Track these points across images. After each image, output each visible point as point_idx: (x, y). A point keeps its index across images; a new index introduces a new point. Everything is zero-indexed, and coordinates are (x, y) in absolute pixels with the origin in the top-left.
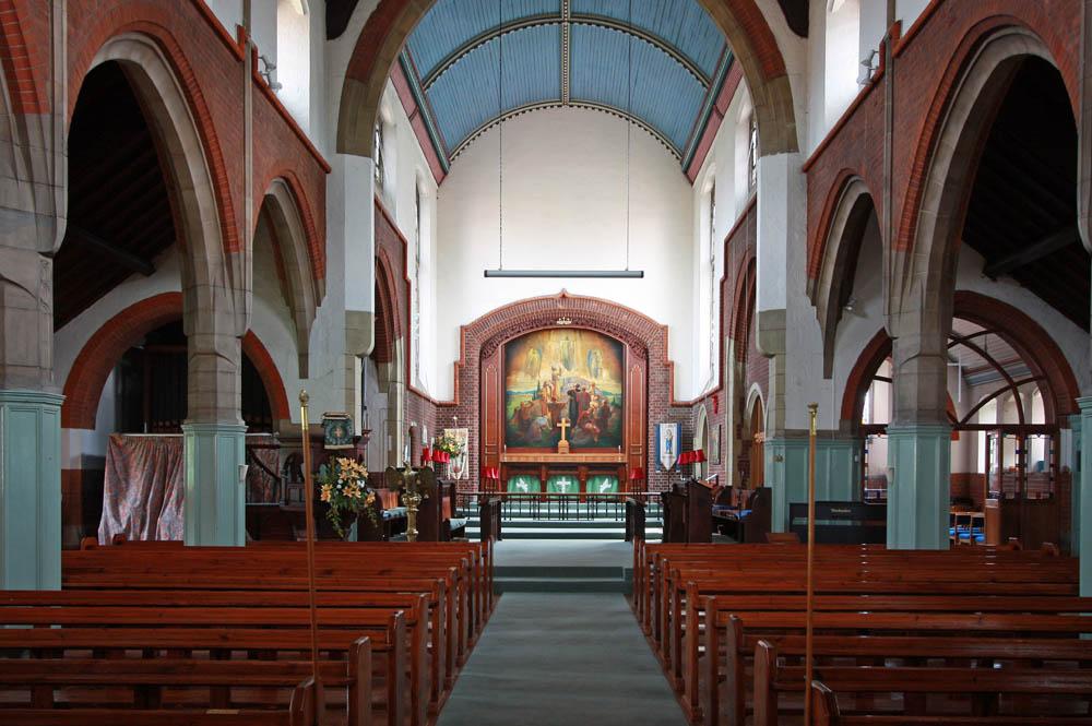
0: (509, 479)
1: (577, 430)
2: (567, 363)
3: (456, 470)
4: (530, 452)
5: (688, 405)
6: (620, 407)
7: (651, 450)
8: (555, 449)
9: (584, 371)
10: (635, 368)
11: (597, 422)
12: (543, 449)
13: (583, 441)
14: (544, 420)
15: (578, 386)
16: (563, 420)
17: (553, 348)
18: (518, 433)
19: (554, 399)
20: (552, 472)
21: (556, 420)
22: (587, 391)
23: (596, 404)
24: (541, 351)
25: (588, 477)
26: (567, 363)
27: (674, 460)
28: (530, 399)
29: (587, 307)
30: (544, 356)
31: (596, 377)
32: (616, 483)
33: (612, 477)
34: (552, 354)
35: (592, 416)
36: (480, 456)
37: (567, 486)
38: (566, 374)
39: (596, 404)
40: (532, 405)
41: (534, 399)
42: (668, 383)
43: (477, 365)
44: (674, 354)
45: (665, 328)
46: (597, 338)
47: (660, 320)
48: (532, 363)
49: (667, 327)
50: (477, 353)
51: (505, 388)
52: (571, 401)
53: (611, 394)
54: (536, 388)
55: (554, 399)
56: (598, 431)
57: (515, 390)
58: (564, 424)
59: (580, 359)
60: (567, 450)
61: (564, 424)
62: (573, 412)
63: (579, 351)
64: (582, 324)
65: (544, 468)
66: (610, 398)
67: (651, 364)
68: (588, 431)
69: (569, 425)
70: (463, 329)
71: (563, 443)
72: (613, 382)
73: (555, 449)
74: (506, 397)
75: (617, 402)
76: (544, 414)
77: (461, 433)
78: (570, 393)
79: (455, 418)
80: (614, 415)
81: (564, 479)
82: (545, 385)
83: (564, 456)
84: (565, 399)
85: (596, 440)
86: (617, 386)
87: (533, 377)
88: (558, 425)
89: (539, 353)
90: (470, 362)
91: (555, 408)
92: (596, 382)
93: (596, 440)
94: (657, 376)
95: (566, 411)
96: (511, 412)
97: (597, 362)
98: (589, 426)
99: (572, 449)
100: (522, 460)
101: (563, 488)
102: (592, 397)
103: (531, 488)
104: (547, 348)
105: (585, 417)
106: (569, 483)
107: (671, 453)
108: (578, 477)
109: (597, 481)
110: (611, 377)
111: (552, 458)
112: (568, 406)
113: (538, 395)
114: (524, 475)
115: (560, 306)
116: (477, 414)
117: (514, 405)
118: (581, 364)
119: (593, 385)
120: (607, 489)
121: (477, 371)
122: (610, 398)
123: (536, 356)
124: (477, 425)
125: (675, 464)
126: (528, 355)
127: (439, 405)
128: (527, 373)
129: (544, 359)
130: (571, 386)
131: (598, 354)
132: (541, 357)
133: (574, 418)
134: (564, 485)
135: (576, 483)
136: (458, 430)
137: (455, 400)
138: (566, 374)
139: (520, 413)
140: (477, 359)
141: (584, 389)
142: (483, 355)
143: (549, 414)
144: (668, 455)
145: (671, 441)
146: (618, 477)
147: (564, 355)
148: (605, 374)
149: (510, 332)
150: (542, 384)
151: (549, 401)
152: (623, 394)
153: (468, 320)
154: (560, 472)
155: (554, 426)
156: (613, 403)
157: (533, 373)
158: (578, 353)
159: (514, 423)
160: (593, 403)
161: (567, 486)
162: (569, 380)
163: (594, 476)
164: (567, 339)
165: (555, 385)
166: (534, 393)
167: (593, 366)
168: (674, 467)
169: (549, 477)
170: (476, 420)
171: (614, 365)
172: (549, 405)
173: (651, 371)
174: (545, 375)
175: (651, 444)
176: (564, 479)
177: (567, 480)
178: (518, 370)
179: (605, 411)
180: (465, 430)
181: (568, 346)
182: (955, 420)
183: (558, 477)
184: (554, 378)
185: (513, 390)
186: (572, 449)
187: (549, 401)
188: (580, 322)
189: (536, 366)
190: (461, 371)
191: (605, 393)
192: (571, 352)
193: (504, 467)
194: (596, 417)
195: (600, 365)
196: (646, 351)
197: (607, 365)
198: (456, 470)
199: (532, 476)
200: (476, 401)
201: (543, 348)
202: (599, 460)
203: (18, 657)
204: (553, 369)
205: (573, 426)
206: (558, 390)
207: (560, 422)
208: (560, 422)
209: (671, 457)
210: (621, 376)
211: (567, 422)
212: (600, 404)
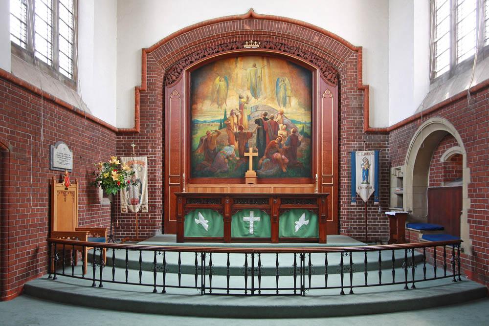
0: (185, 213)
1: (264, 160)
2: (255, 92)
3: (134, 202)
4: (215, 183)
5: (385, 132)
6: (310, 136)
7: (344, 181)
8: (242, 180)
9: (272, 99)
10: (326, 96)
11: (286, 152)
12: (229, 180)
13: (272, 171)
14: (230, 150)
15: (266, 114)
16: (251, 149)
17: (240, 76)
18: (205, 162)
19: (241, 128)
20: (238, 205)
21: (244, 149)
22: (275, 120)
23: (285, 133)
24: (228, 79)
25: (281, 212)
26: (255, 92)
27: (372, 191)
28: (217, 129)
29: (276, 27)
30: (231, 84)
31: (284, 105)
32: (314, 219)
33: (310, 213)
34: (240, 81)
35: (281, 146)
36: (163, 186)
37: (255, 222)
38: (253, 102)
39: (285, 133)
40: (219, 133)
41: (221, 128)
42: (364, 108)
43: (159, 91)
44: (370, 78)
45: (359, 50)
46: (285, 65)
47: (354, 42)
48: (218, 91)
49: (361, 48)
50: (161, 79)
51: (191, 118)
52: (258, 129)
53: (300, 123)
54: (223, 117)
55: (241, 128)
56: (287, 161)
57: (201, 119)
58: (251, 154)
59: (268, 85)
60: (254, 180)
61: (251, 154)
62: (261, 142)
63: (267, 78)
64: (270, 48)
65: (227, 201)
66: (299, 127)
67: (343, 89)
68: (276, 161)
69: (256, 154)
70: (145, 52)
71: (251, 173)
72: (302, 111)
73: (242, 180)
74: (192, 126)
75: (305, 131)
76: (231, 143)
77: (139, 163)
78: (258, 122)
79: (133, 145)
80: (302, 144)
81: (252, 213)
82: (232, 114)
83: (251, 187)
84: (253, 128)
85: (284, 170)
86: (305, 115)
87: (220, 105)
88: (246, 154)
89: (225, 79)
90: (151, 87)
91: (242, 137)
92: (285, 110)
93: (284, 170)
94: (351, 101)
95: (253, 140)
96: (197, 142)
97: (285, 90)
98: (277, 155)
99: (260, 180)
100: (209, 191)
101: (251, 225)
102: (281, 126)
103: (212, 226)
104: (234, 75)
105: (273, 146)
106: (258, 219)
107: (368, 183)
108: (269, 212)
109: (292, 216)
110: (299, 104)
111: (239, 189)
112: (255, 135)
113: (225, 124)
114: (203, 209)
115: (247, 28)
116: (159, 142)
117: (200, 134)
118: (268, 90)
119: (282, 113)
120: (304, 227)
121: (160, 97)
122: (299, 127)
123: (223, 84)
124: (159, 154)
125: (373, 195)
126: (215, 82)
127: (119, 133)
128: (213, 101)
129: (231, 87)
130: (259, 115)
131: (287, 81)
132: (228, 85)
133: (261, 147)
134: (252, 222)
135: (267, 219)
136: (136, 159)
137: (135, 127)
138: (253, 102)
139: (207, 142)
140: (160, 84)
141: (272, 118)
142: (167, 81)
143: (236, 144)
144: (365, 186)
145: (368, 170)
146: (317, 212)
147: (252, 83)
148: (294, 102)
149: (194, 56)
150: (228, 113)
151: (236, 130)
152: (313, 124)
153: (150, 43)
154: (249, 206)
155: (242, 156)
156: (302, 133)
157: (219, 100)
158: (266, 79)
159: (200, 154)
160: (281, 132)
161: (255, 222)
162: (256, 108)
163: (288, 211)
164: (255, 66)
165: (242, 113)
166: (221, 121)
167: (281, 94)
168: (372, 198)
169: (233, 212)
170: (159, 149)
171: (303, 92)
172: (236, 135)
173: (343, 96)
174: (232, 103)
175: (344, 173)
176: (252, 213)
177: (255, 216)
178: (205, 98)
179: (293, 141)
180: (145, 159)
181: (256, 74)
182: (359, 199)
183: (194, 211)
184: (242, 107)
185: (200, 118)
186: (260, 180)
187: (236, 130)
188: (268, 46)
189: (223, 93)
190: (142, 96)
191: (294, 122)
192: (259, 79)
193: (180, 200)
194: (284, 146)
195: (289, 92)
196: (338, 77)
197: (296, 93)
198: (134, 202)
199: (214, 210)
200: (159, 129)
201: (230, 75)
202: (297, 191)
203: (88, 261)
204: (240, 98)
205: (260, 156)
206: (245, 118)
207: (248, 152)
208: (248, 152)
209: (368, 188)
210: (311, 106)
211: (254, 151)
212: (288, 132)
